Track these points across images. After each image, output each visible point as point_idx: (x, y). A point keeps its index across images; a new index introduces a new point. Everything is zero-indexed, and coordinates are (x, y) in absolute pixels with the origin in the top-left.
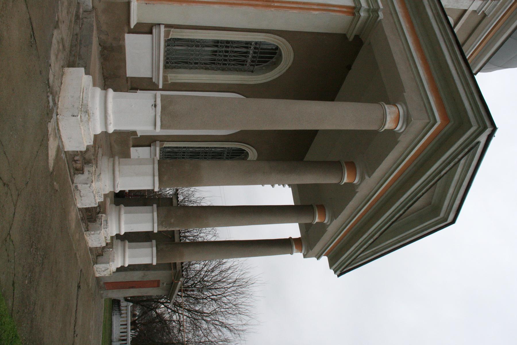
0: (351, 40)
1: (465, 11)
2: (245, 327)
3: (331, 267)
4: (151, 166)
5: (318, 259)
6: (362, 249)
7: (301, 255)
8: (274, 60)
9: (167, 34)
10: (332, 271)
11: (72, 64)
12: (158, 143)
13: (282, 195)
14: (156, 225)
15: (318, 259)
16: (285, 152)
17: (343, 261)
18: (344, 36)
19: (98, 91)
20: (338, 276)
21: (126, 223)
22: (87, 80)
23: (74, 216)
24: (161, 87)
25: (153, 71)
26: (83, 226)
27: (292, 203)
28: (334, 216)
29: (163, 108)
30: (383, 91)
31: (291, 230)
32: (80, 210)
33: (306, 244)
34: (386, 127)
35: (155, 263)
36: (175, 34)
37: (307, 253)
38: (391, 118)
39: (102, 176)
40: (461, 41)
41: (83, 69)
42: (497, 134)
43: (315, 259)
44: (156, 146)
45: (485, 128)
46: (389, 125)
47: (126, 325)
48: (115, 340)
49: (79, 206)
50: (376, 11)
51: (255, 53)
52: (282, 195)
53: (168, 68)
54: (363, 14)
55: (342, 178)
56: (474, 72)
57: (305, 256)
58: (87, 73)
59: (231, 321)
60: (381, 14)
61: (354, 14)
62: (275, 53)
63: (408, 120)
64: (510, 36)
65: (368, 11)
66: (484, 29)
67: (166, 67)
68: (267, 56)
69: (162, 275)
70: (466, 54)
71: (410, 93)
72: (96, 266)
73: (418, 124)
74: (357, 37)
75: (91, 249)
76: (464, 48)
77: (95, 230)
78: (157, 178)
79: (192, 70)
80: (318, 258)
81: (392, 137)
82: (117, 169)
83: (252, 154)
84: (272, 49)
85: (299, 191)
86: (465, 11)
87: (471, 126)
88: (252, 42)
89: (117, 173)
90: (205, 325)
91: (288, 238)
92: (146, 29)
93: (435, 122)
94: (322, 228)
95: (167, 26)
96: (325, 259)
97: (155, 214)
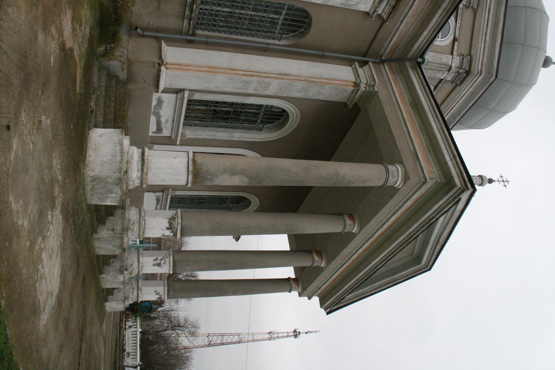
0: (350, 107)
5: (309, 298)
8: (281, 121)
13: (280, 242)
15: (309, 298)
16: (284, 202)
17: (332, 302)
18: (345, 104)
20: (328, 313)
24: (178, 143)
25: (172, 128)
27: (289, 250)
30: (377, 151)
31: (288, 272)
33: (302, 283)
36: (197, 97)
37: (303, 292)
38: (396, 175)
40: (439, 102)
42: (476, 194)
45: (467, 188)
51: (265, 114)
52: (280, 242)
53: (186, 125)
54: (362, 87)
56: (450, 128)
57: (300, 295)
62: (282, 116)
68: (275, 117)
70: (443, 113)
73: (414, 180)
74: (355, 104)
76: (442, 108)
79: (207, 128)
84: (279, 112)
85: (294, 239)
88: (263, 105)
91: (287, 277)
94: (318, 271)
95: (191, 90)
96: (316, 300)
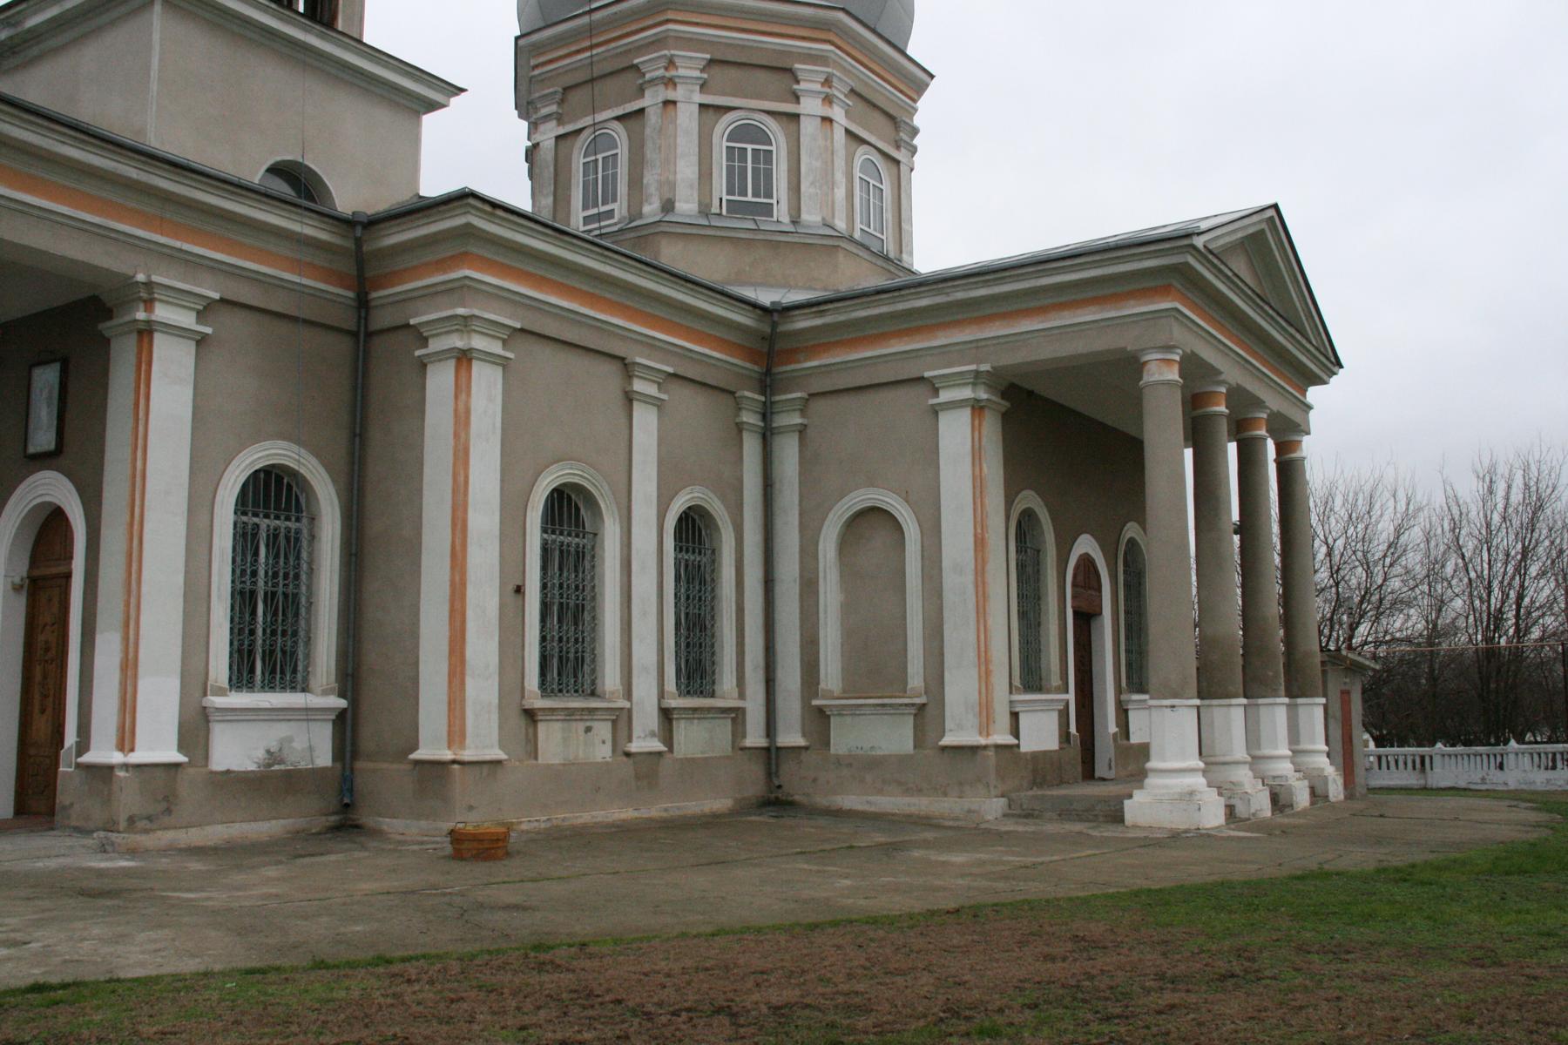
1: (847, 131)
2: (1401, 495)
3: (1325, 383)
4: (1233, 710)
6: (1304, 342)
7: (1306, 440)
9: (1018, 691)
10: (1334, 379)
11: (1117, 817)
12: (1124, 697)
14: (1279, 700)
19: (1151, 781)
20: (1341, 366)
21: (1276, 748)
22: (1139, 796)
23: (1281, 820)
26: (1288, 811)
28: (1258, 403)
29: (1175, 696)
32: (1273, 811)
33: (1288, 432)
34: (1177, 377)
35: (1323, 700)
38: (1162, 372)
39: (1233, 779)
41: (1127, 803)
43: (1312, 413)
44: (1129, 701)
46: (1173, 374)
47: (1379, 758)
48: (1422, 782)
49: (1269, 814)
50: (977, 373)
55: (1221, 414)
57: (1308, 433)
58: (1130, 796)
59: (1385, 529)
60: (985, 367)
61: (982, 408)
63: (1169, 348)
64: (874, 31)
65: (974, 384)
66: (866, 84)
67: (1040, 690)
69: (1336, 683)
71: (1127, 341)
72: (1332, 798)
73: (1178, 333)
75: (1312, 803)
77: (1291, 794)
78: (1215, 702)
80: (1310, 407)
81: (1193, 368)
82: (1222, 759)
83: (1131, 530)
86: (847, 131)
87: (1187, 264)
89: (1228, 759)
90: (1395, 584)
92: (195, 729)
93: (1177, 310)
96: (1314, 394)
97: (1260, 701)
